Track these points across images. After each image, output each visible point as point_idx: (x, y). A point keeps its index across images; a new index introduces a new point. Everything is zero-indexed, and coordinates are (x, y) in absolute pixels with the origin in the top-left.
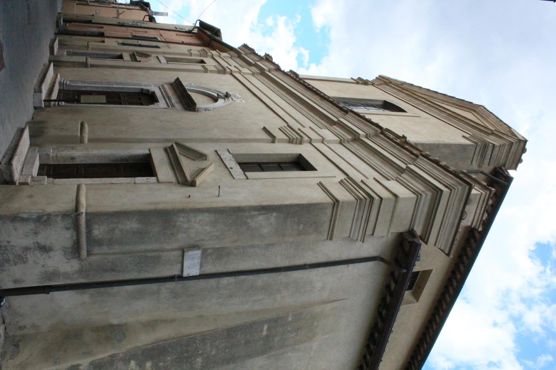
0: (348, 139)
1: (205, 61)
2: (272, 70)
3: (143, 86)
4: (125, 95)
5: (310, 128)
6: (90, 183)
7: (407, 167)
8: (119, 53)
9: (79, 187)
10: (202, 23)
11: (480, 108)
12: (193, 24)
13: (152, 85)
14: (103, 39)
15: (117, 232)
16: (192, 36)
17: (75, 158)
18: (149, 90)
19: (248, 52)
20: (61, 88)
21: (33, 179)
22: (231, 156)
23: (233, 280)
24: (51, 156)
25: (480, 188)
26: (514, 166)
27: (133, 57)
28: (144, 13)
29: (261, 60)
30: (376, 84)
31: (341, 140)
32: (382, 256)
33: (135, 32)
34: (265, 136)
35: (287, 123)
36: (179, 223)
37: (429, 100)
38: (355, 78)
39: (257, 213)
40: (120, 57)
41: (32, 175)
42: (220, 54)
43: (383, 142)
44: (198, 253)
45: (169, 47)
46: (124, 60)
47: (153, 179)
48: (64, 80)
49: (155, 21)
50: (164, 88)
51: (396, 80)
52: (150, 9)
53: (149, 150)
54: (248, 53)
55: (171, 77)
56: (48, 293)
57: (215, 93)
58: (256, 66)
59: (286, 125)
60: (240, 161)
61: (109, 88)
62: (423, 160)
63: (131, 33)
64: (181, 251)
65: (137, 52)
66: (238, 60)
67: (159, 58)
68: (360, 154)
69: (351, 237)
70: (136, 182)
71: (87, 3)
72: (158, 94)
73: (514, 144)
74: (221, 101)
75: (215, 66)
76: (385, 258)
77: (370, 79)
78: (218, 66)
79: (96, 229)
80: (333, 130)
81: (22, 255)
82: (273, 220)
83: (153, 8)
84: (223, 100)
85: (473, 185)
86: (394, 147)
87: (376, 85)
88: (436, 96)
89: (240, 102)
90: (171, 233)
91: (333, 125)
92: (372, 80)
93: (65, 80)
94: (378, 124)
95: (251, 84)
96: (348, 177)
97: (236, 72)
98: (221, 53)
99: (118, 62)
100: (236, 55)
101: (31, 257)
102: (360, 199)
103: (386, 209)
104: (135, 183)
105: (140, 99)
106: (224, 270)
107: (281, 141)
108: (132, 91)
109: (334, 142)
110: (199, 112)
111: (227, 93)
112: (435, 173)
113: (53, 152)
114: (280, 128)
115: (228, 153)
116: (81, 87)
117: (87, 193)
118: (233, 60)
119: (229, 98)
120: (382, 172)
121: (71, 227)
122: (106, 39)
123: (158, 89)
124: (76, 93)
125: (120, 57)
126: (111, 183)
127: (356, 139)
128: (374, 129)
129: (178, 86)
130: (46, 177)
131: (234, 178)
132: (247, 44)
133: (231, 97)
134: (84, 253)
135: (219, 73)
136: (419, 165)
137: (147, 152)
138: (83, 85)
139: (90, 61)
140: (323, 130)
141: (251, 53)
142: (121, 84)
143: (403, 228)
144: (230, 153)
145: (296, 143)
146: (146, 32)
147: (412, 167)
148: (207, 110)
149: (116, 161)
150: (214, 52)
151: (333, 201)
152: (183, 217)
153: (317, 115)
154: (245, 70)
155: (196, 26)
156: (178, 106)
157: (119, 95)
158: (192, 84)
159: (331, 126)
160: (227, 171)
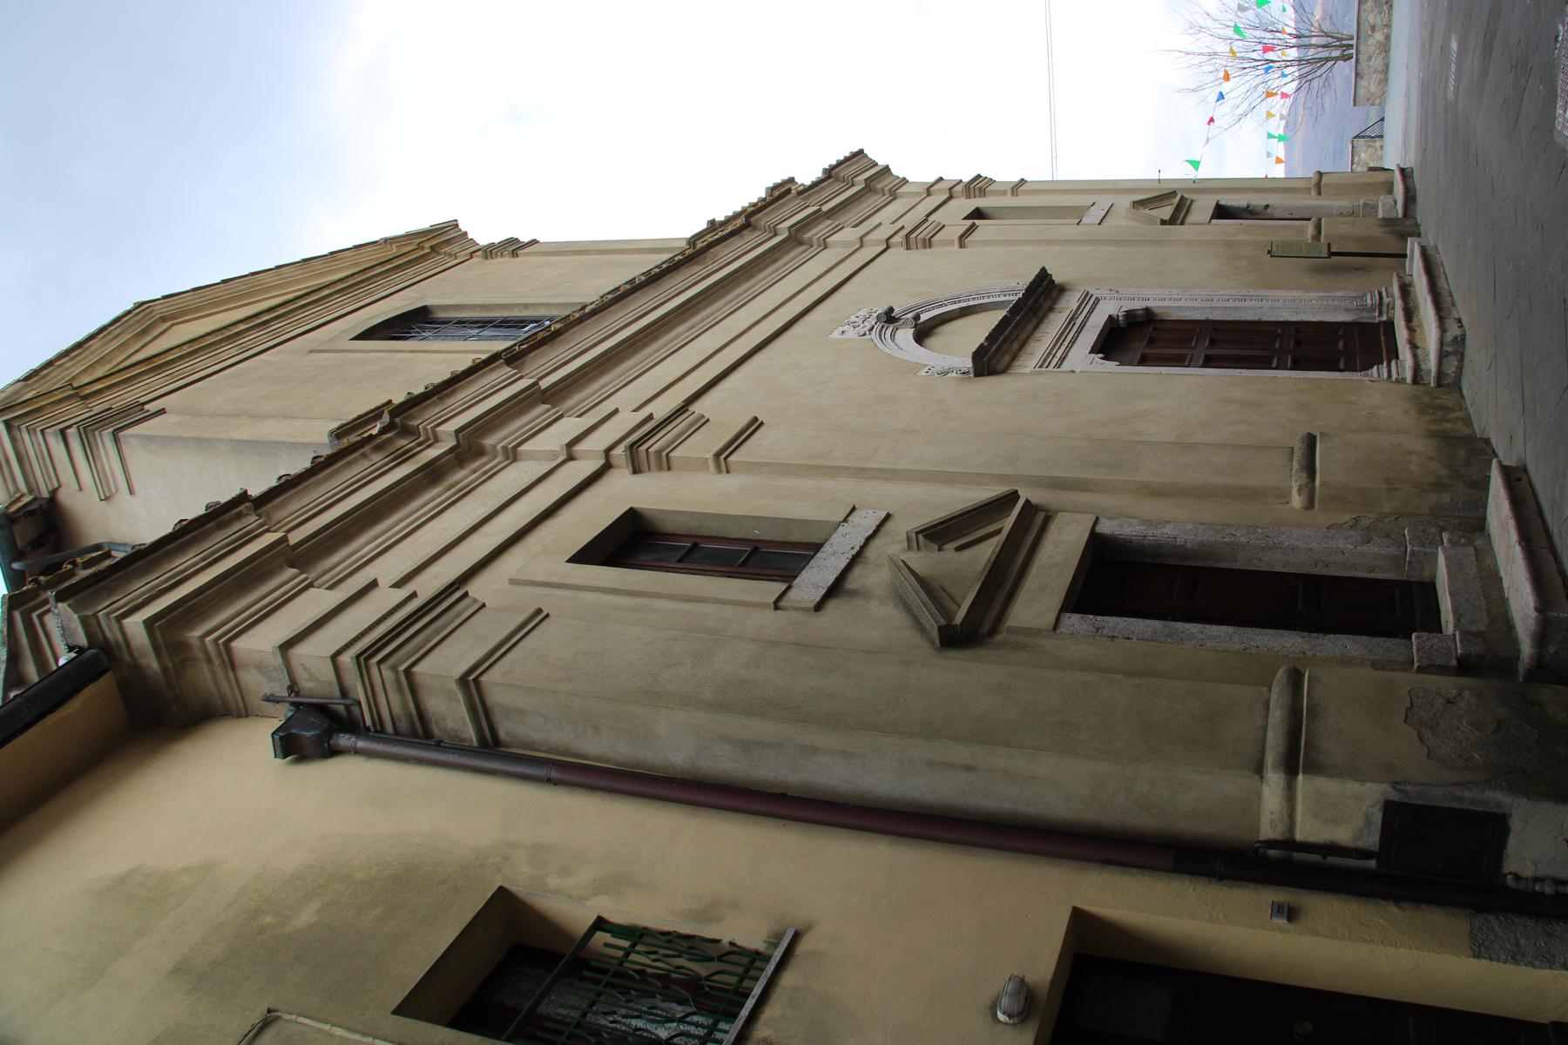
37: (121, 366)
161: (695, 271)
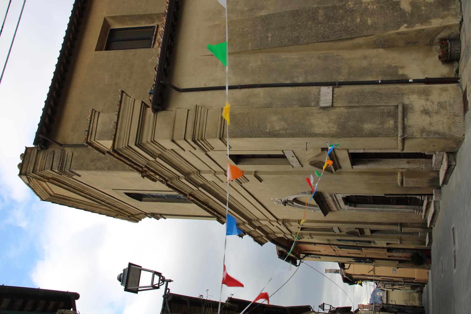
0: (194, 175)
2: (242, 224)
3: (354, 209)
4: (369, 202)
5: (277, 226)
6: (395, 150)
7: (155, 159)
8: (373, 234)
9: (403, 149)
10: (294, 263)
11: (46, 198)
12: (302, 262)
14: (388, 246)
15: (378, 122)
16: (306, 250)
17: (407, 163)
18: (350, 206)
20: (421, 207)
21: (435, 153)
22: (291, 164)
23: (295, 80)
24: (424, 165)
25: (93, 144)
26: (28, 151)
27: (362, 232)
28: (348, 271)
29: (250, 232)
30: (143, 215)
32: (177, 92)
33: (359, 253)
34: (261, 176)
35: (241, 186)
36: (336, 126)
37: (99, 204)
38: (162, 219)
39: (280, 132)
40: (372, 231)
41: (436, 155)
42: (285, 236)
44: (322, 104)
45: (328, 240)
46: (369, 229)
47: (351, 151)
48: (419, 213)
49: (339, 263)
50: (337, 208)
51: (122, 219)
52: (343, 276)
53: (352, 168)
55: (330, 216)
56: (426, 78)
57: (294, 205)
58: (254, 227)
60: (285, 159)
61: (382, 208)
62: (142, 165)
63: (362, 252)
64: (334, 106)
65: (359, 236)
67: (339, 231)
68: (187, 164)
69: (206, 110)
70: (363, 150)
71: (404, 280)
72: (342, 203)
73: (31, 171)
74: (291, 198)
75: (291, 225)
76: (174, 90)
77: (147, 218)
79: (392, 125)
80: (204, 180)
81: (441, 109)
82: (269, 126)
83: (338, 278)
84: (289, 199)
85: (111, 150)
86: (160, 171)
87: (143, 214)
88: (108, 212)
89: (274, 199)
90: (341, 119)
91: (203, 184)
92: (146, 217)
93: (418, 214)
96: (241, 184)
97: (273, 221)
99: (375, 227)
101: (435, 107)
102: (202, 140)
103: (180, 132)
104: (364, 149)
105: (357, 199)
106: (302, 88)
107: (249, 173)
109: (205, 172)
111: (285, 205)
112: (137, 157)
113: (423, 167)
114: (248, 181)
115: (293, 165)
116: (405, 208)
117: (398, 146)
120: (174, 154)
121: (408, 128)
122: (385, 246)
123: (342, 207)
124: (409, 203)
126: (381, 149)
127: (187, 175)
129: (325, 209)
130: (426, 154)
131: (292, 151)
133: (282, 202)
134: (400, 108)
135: (288, 220)
137: (354, 167)
138: (403, 210)
139: (398, 228)
140: (211, 180)
142: (372, 211)
143: (161, 114)
144: (292, 165)
146: (348, 253)
147: (151, 159)
148: (304, 192)
149: (377, 161)
150: (290, 237)
151: (223, 139)
152: (332, 131)
153: (213, 190)
154: (264, 223)
155: (299, 261)
156: (327, 195)
157: (374, 202)
158: (313, 211)
159: (204, 184)
160: (296, 155)
161: (211, 203)
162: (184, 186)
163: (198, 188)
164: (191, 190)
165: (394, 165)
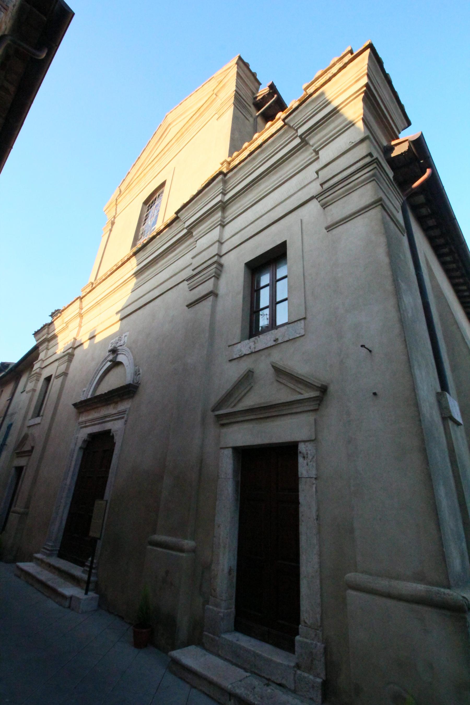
1: (49, 375)
5: (193, 258)
13: (77, 435)
19: (47, 330)
24: (226, 611)
31: (220, 224)
43: (240, 174)
47: (25, 468)
48: (44, 548)
54: (48, 331)
57: (106, 363)
59: (186, 283)
66: (54, 343)
68: (250, 203)
78: (61, 362)
94: (184, 203)
95: (241, 229)
96: (316, 197)
97: (41, 364)
98: (40, 358)
100: (46, 343)
102: (373, 175)
108: (79, 462)
110: (139, 382)
114: (190, 289)
118: (51, 348)
119: (118, 350)
125: (19, 470)
128: (218, 183)
132: (35, 332)
136: (301, 122)
141: (49, 328)
145: (221, 271)
151: (379, 205)
162: (217, 192)
163: (186, 228)
164: (187, 218)
165: (227, 538)
